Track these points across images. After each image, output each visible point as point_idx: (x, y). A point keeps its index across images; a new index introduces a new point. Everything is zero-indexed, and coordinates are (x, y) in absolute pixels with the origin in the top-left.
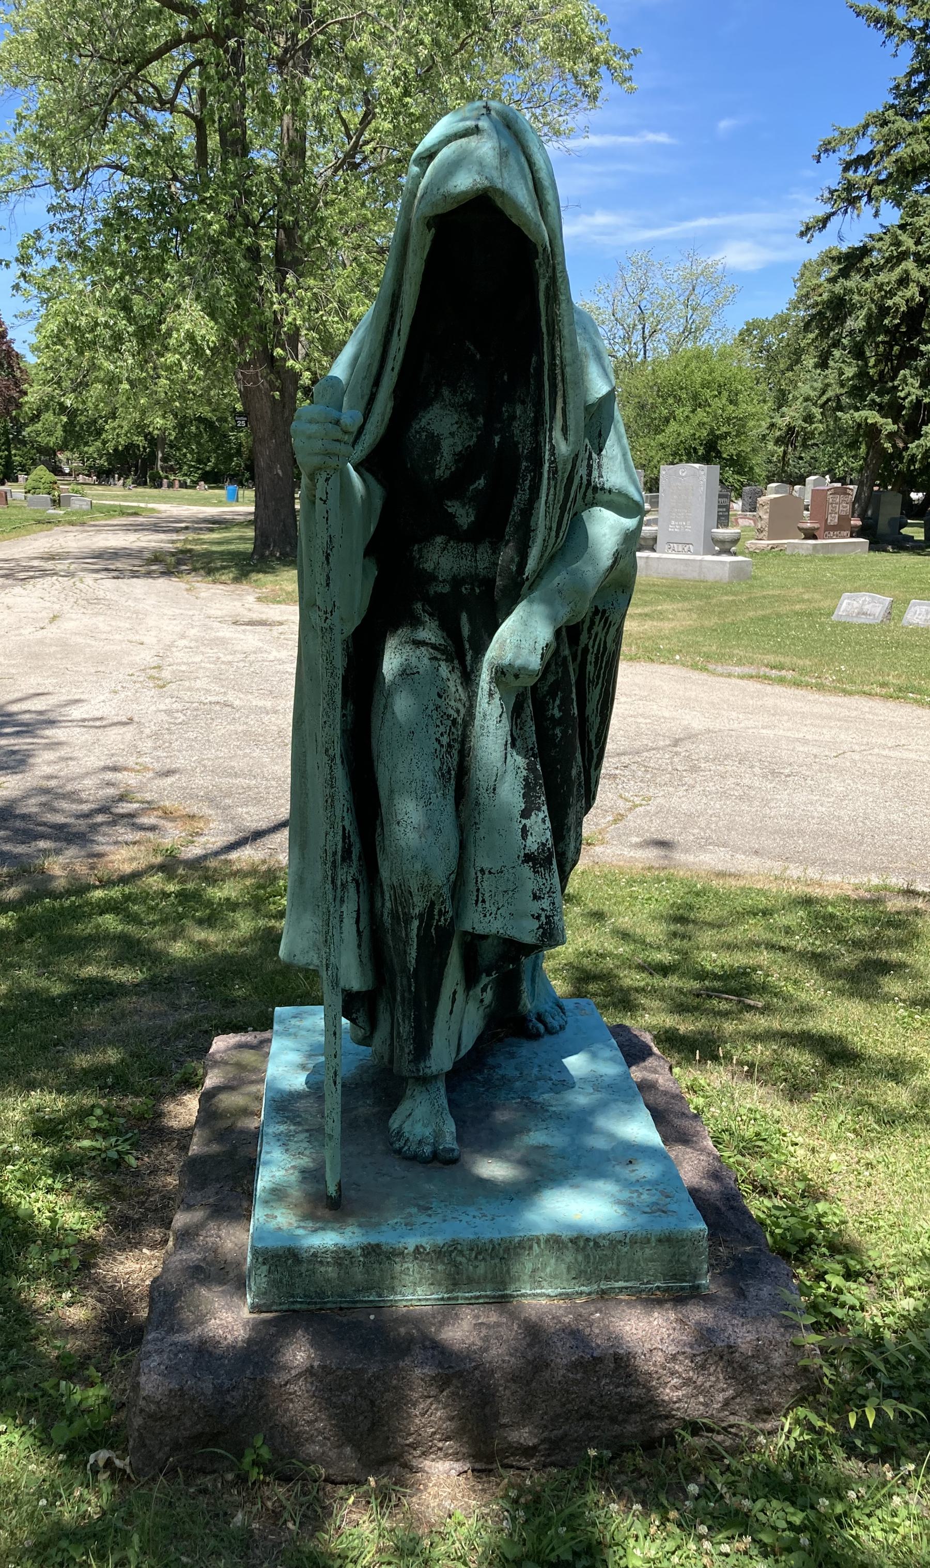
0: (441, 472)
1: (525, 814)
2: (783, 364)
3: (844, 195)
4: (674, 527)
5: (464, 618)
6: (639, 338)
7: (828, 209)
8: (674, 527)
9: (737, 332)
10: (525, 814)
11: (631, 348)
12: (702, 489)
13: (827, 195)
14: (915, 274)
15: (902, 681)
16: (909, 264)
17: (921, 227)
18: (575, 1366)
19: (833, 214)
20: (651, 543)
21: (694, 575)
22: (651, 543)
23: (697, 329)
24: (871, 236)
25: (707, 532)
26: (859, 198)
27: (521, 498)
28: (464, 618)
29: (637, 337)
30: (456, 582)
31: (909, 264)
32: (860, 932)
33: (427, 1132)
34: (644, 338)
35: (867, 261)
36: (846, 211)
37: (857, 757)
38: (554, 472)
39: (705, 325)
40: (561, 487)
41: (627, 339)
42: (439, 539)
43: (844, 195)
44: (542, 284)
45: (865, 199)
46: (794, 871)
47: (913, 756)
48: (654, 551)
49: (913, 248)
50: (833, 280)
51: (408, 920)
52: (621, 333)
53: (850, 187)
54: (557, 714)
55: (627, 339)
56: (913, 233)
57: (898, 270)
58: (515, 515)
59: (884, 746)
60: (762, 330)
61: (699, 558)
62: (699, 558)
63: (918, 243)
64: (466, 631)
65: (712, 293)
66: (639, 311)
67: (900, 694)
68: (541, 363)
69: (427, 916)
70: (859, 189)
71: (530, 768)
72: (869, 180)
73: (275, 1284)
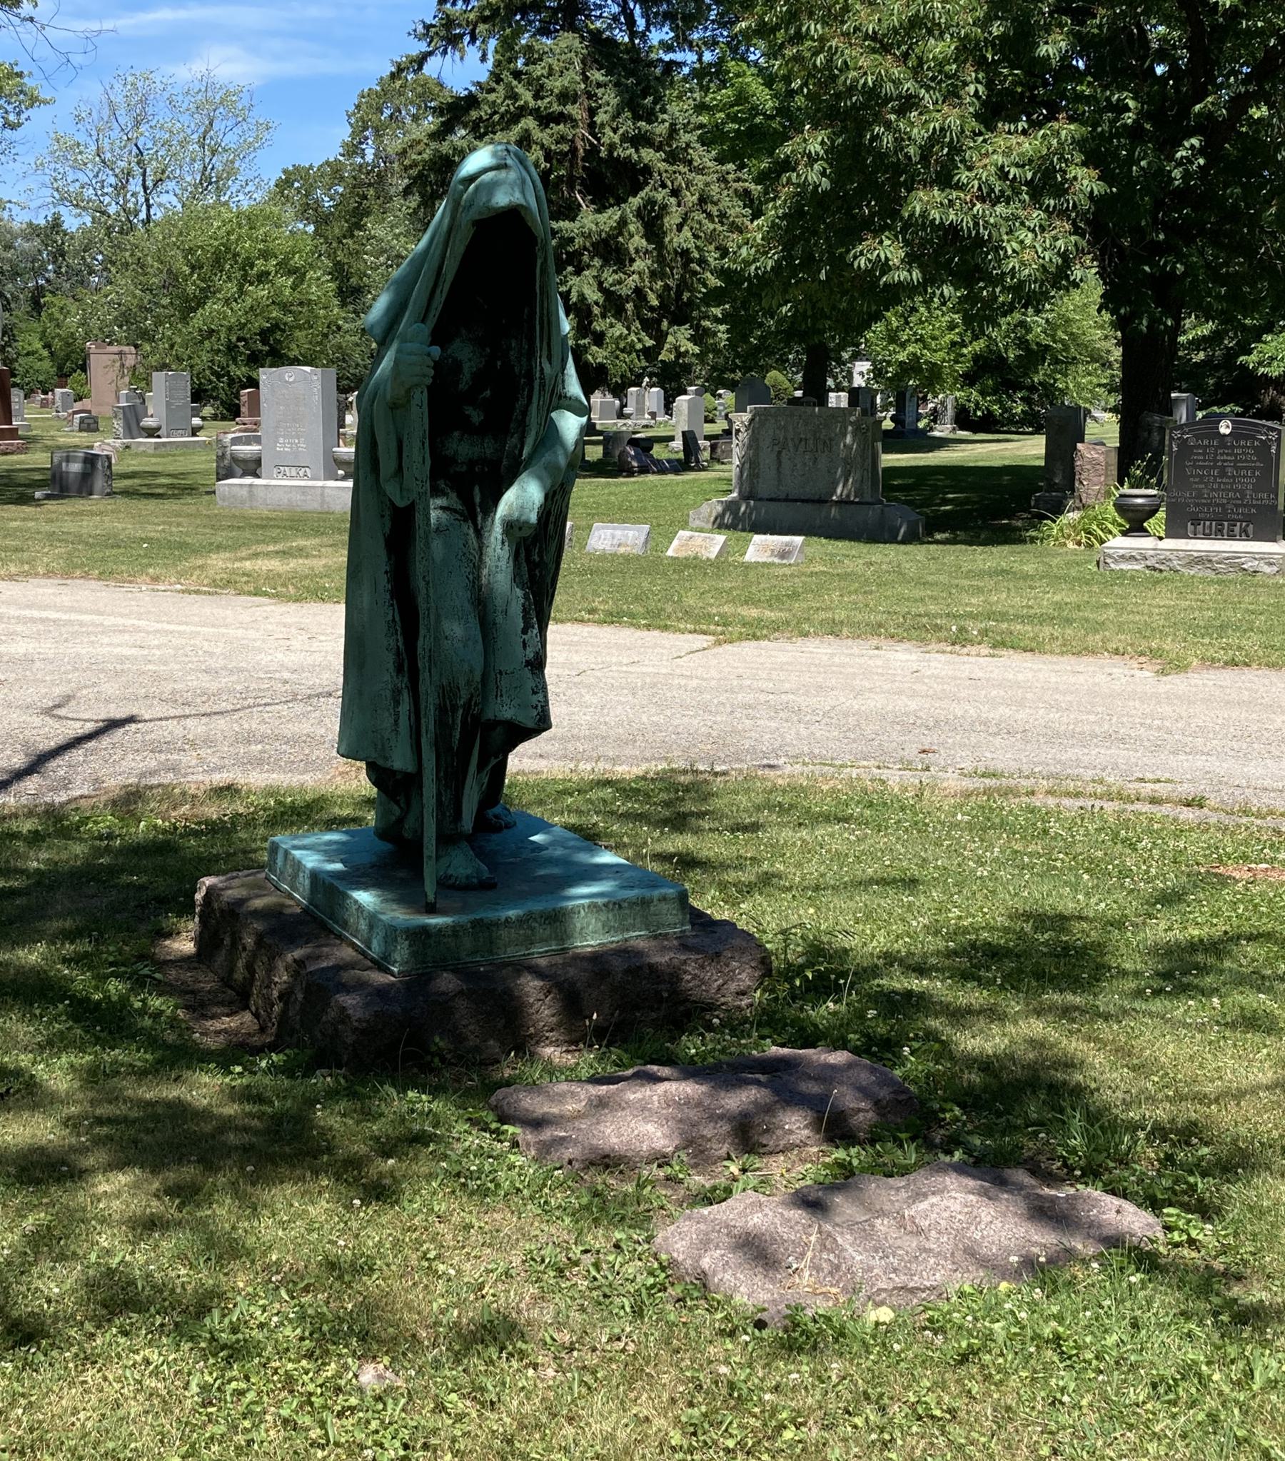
0: (463, 386)
1: (524, 631)
2: (337, 229)
3: (443, 33)
4: (283, 446)
5: (477, 489)
6: (140, 189)
7: (423, 47)
8: (283, 446)
9: (272, 183)
10: (524, 631)
11: (126, 201)
12: (317, 397)
13: (420, 29)
14: (537, 134)
15: (609, 606)
16: (529, 123)
17: (539, 78)
18: (628, 971)
19: (430, 54)
20: (253, 466)
21: (315, 506)
22: (253, 466)
23: (219, 178)
24: (479, 84)
25: (328, 453)
26: (461, 36)
27: (522, 402)
28: (477, 489)
29: (135, 185)
30: (471, 463)
31: (529, 123)
32: (664, 796)
33: (469, 871)
34: (145, 188)
35: (474, 114)
36: (445, 52)
37: (599, 674)
38: (542, 385)
39: (231, 172)
40: (547, 396)
41: (121, 188)
42: (456, 434)
43: (443, 33)
44: (539, 262)
45: (467, 38)
46: (585, 767)
47: (650, 669)
48: (258, 477)
49: (532, 103)
50: (434, 136)
51: (454, 708)
52: (112, 180)
53: (449, 22)
54: (536, 558)
55: (121, 188)
56: (529, 84)
57: (516, 130)
58: (517, 413)
59: (621, 664)
60: (306, 181)
61: (320, 483)
62: (320, 483)
63: (537, 96)
64: (478, 499)
65: (237, 130)
66: (135, 151)
67: (613, 618)
68: (533, 313)
69: (467, 707)
70: (460, 26)
71: (526, 597)
72: (472, 16)
73: (414, 954)
